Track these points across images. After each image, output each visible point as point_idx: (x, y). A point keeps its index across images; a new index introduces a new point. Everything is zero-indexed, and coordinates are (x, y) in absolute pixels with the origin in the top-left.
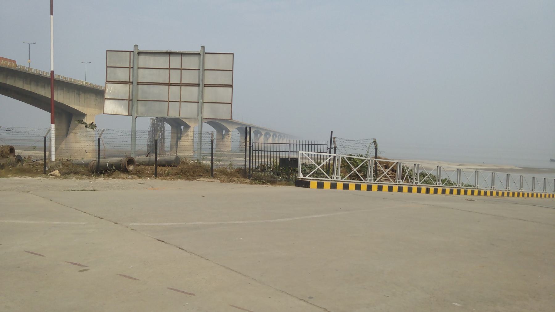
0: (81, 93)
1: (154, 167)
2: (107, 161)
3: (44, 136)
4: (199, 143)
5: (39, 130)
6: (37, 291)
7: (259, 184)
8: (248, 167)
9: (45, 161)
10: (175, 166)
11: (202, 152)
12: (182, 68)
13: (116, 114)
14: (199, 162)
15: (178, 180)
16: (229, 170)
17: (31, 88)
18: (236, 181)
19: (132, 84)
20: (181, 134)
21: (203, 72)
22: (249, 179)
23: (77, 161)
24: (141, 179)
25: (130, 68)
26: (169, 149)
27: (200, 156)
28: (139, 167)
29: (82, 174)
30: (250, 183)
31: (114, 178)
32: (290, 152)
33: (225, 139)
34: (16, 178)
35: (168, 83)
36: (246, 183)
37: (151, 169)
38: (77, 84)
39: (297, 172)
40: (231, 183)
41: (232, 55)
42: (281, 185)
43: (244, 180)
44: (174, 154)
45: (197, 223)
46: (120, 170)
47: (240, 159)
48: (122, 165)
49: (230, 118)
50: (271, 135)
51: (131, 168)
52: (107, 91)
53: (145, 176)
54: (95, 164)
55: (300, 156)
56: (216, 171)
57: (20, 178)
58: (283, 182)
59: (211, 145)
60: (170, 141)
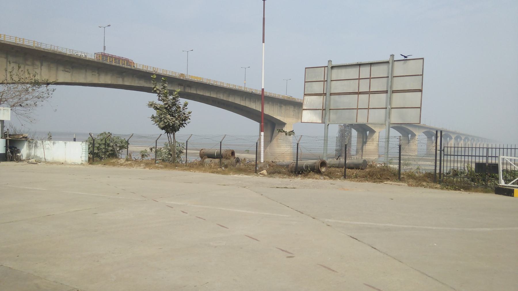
0: (282, 105)
1: (343, 170)
2: (304, 163)
3: (256, 142)
4: (386, 147)
5: (252, 137)
6: (255, 270)
7: (451, 189)
8: (438, 171)
9: (256, 162)
10: (362, 168)
11: (389, 156)
12: (372, 77)
13: (311, 122)
14: (386, 165)
15: (366, 182)
16: (417, 174)
17: (246, 103)
18: (425, 185)
19: (326, 95)
20: (366, 139)
21: (392, 79)
22: (439, 183)
23: (280, 163)
24: (331, 180)
25: (324, 81)
26: (355, 153)
27: (387, 160)
28: (330, 169)
29: (284, 174)
30: (440, 188)
31: (309, 178)
32: (487, 156)
33: (411, 143)
34: (236, 175)
35: (358, 92)
36: (436, 188)
37: (341, 171)
38: (280, 98)
39: (498, 179)
40: (419, 188)
41: (422, 60)
42: (476, 192)
43: (433, 185)
44: (359, 158)
45: (388, 225)
46: (314, 171)
47: (429, 163)
48: (316, 167)
49: (419, 123)
50: (463, 139)
51: (323, 170)
52: (305, 103)
53: (337, 177)
54: (294, 165)
55: (501, 162)
56: (404, 175)
57: (238, 176)
58: (480, 189)
59: (398, 149)
60: (356, 145)
